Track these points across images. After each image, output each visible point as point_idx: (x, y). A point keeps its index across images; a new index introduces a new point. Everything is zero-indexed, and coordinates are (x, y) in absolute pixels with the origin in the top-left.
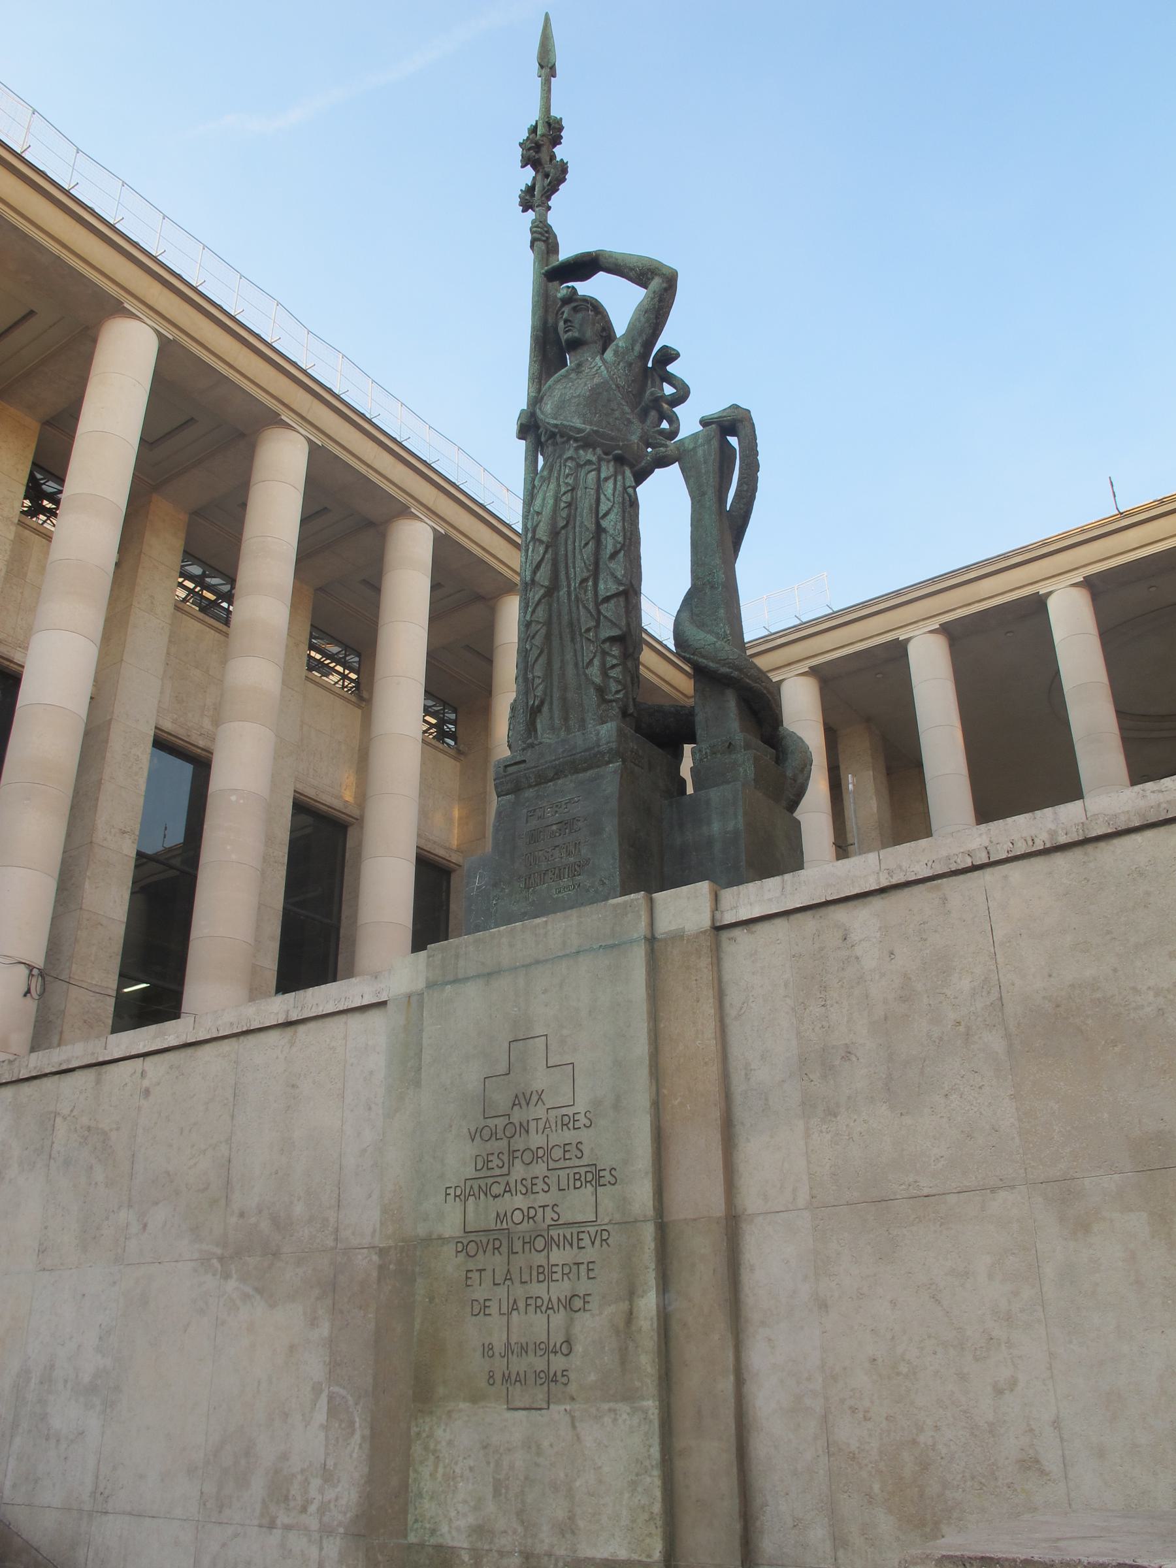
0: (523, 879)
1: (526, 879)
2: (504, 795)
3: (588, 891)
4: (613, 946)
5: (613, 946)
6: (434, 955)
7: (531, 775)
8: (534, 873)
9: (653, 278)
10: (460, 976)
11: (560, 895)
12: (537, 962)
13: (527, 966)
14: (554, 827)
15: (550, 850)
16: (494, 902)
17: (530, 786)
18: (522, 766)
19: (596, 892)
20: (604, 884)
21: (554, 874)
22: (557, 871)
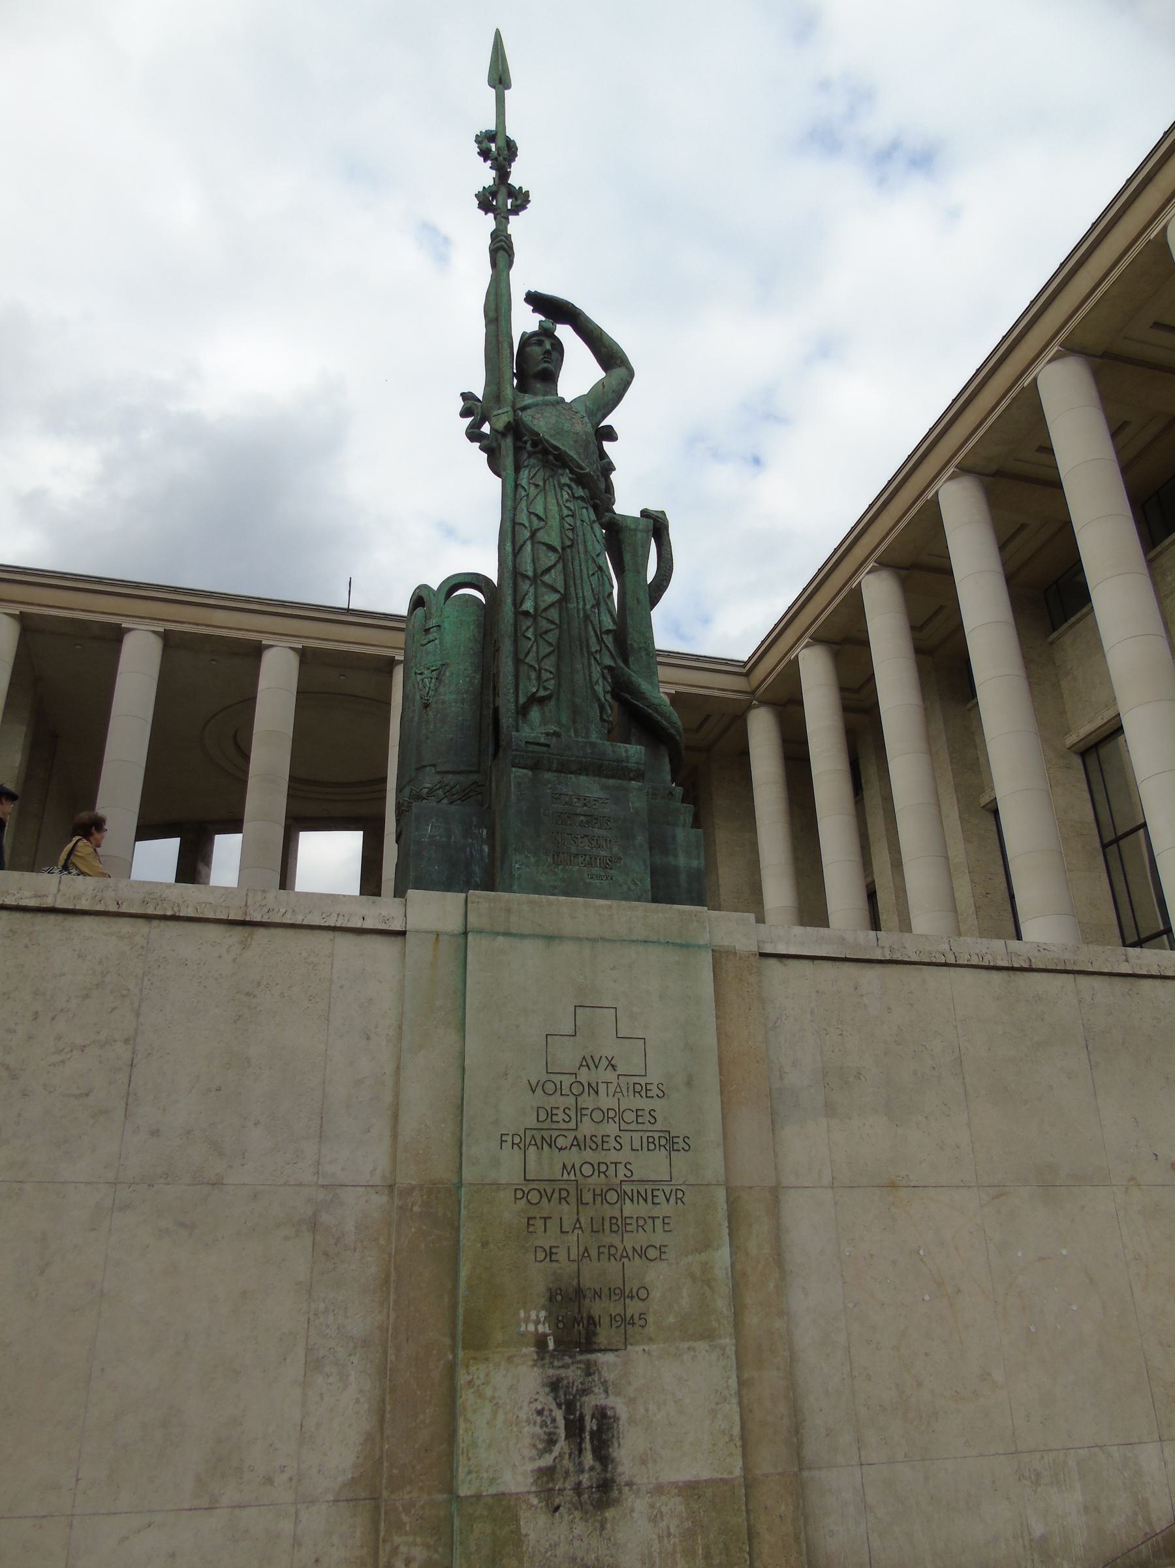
0: (551, 854)
1: (553, 855)
2: (519, 767)
3: (620, 886)
4: (681, 946)
5: (681, 946)
6: (478, 902)
7: (554, 761)
8: (563, 853)
9: (620, 366)
10: (513, 931)
11: (592, 881)
12: (603, 939)
13: (594, 940)
14: (582, 818)
15: (579, 836)
16: (517, 866)
17: (549, 770)
18: (544, 749)
19: (629, 889)
20: (636, 884)
21: (585, 860)
22: (588, 858)
